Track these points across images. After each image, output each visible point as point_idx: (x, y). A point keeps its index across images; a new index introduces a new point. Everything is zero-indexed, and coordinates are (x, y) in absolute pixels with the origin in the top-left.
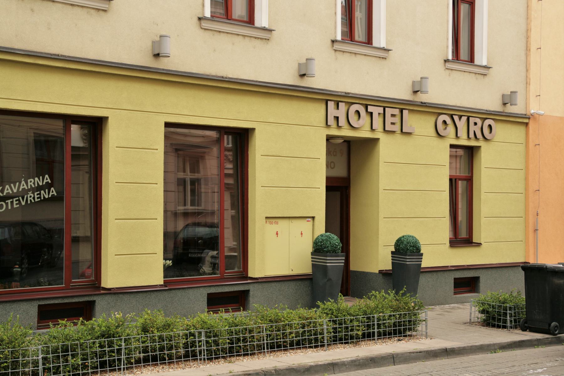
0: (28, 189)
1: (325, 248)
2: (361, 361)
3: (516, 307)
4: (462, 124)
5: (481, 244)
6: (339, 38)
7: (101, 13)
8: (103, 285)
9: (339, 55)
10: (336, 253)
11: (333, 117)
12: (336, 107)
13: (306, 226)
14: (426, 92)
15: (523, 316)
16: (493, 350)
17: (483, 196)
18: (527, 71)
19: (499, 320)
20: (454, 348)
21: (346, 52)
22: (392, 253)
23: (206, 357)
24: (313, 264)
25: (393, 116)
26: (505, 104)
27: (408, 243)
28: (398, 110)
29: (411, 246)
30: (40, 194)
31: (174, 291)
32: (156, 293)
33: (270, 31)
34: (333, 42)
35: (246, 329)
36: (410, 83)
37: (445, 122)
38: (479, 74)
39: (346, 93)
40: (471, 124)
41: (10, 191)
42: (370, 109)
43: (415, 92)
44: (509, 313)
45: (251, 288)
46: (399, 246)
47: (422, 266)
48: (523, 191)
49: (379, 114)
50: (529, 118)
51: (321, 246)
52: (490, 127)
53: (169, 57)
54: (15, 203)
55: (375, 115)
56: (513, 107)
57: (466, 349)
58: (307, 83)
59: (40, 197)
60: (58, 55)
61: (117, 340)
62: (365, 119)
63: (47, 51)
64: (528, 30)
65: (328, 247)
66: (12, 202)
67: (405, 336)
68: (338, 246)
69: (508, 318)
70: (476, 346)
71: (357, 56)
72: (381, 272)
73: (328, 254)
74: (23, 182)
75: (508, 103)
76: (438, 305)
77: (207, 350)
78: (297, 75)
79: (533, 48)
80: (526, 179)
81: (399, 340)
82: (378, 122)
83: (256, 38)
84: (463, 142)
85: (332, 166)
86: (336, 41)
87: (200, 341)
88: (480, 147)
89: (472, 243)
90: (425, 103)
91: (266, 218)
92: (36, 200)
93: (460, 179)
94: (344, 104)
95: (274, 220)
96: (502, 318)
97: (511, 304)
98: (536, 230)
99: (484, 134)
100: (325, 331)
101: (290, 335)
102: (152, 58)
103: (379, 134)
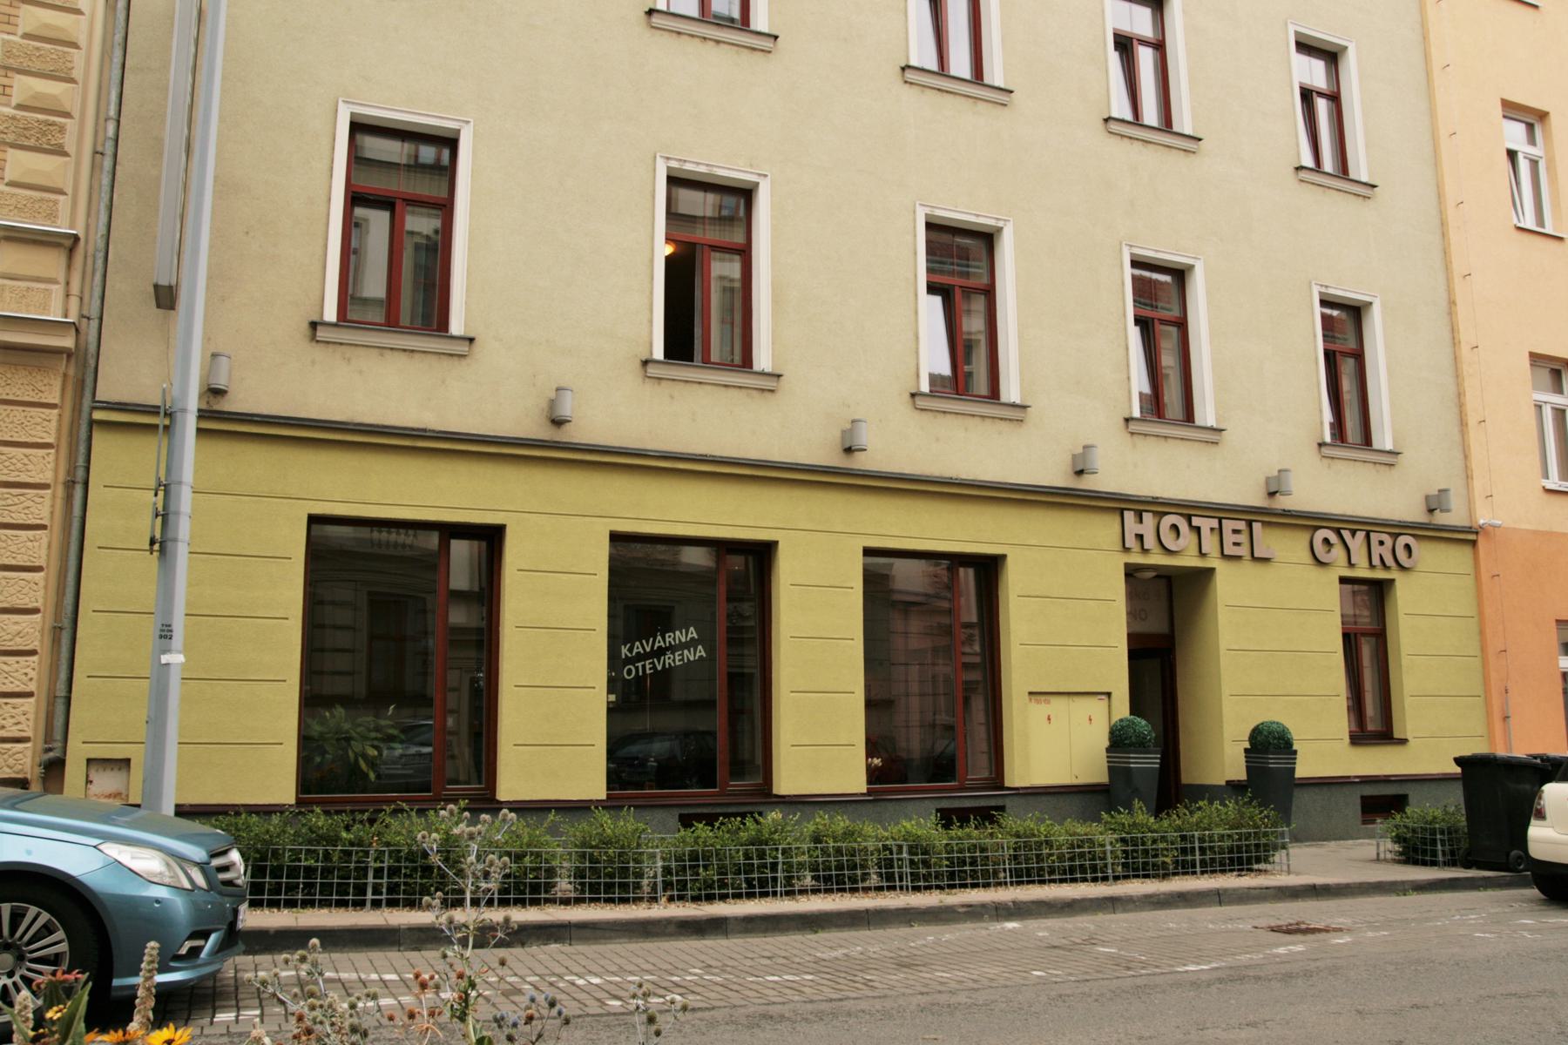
0: (666, 647)
1: (1126, 739)
2: (1162, 896)
3: (1451, 831)
4: (1357, 543)
6: (1137, 413)
7: (767, 394)
8: (775, 791)
9: (1139, 440)
10: (1144, 747)
11: (1134, 536)
12: (1138, 519)
13: (1097, 707)
15: (1464, 845)
16: (1400, 891)
17: (1405, 661)
18: (1466, 457)
19: (1424, 852)
20: (1328, 885)
21: (1149, 435)
22: (1246, 750)
23: (910, 884)
24: (1109, 767)
25: (1236, 532)
26: (1431, 511)
27: (1270, 733)
28: (1244, 522)
29: (1275, 738)
30: (682, 654)
31: (882, 804)
32: (854, 806)
33: (1024, 407)
34: (1127, 420)
35: (975, 846)
36: (1262, 481)
37: (1326, 541)
38: (1380, 463)
39: (1153, 498)
40: (1374, 543)
41: (641, 650)
42: (1196, 521)
43: (1272, 494)
44: (1441, 840)
45: (1008, 803)
46: (1256, 738)
48: (1478, 653)
49: (1212, 529)
50: (1477, 533)
51: (1120, 736)
52: (1408, 547)
53: (865, 450)
54: (648, 667)
55: (1205, 532)
57: (1351, 888)
58: (1088, 483)
59: (682, 660)
60: (706, 456)
61: (771, 849)
62: (1187, 539)
63: (690, 451)
64: (1460, 395)
65: (1131, 737)
66: (644, 666)
67: (1251, 870)
68: (1147, 735)
69: (1439, 847)
70: (1369, 884)
71: (1169, 440)
72: (1228, 783)
73: (1132, 748)
74: (659, 638)
76: (1335, 839)
77: (912, 874)
78: (1070, 471)
79: (1472, 421)
80: (1482, 633)
81: (1239, 875)
82: (1210, 543)
83: (1001, 419)
84: (1363, 572)
85: (1143, 617)
86: (1132, 419)
87: (901, 859)
88: (1392, 581)
89: (1392, 738)
90: (1289, 511)
91: (1030, 693)
92: (678, 663)
93: (1363, 634)
94: (1151, 514)
95: (1043, 698)
96: (1429, 848)
97: (1444, 825)
98: (1506, 718)
99: (1399, 559)
100: (1109, 855)
101: (1048, 858)
102: (842, 455)
103: (1214, 562)
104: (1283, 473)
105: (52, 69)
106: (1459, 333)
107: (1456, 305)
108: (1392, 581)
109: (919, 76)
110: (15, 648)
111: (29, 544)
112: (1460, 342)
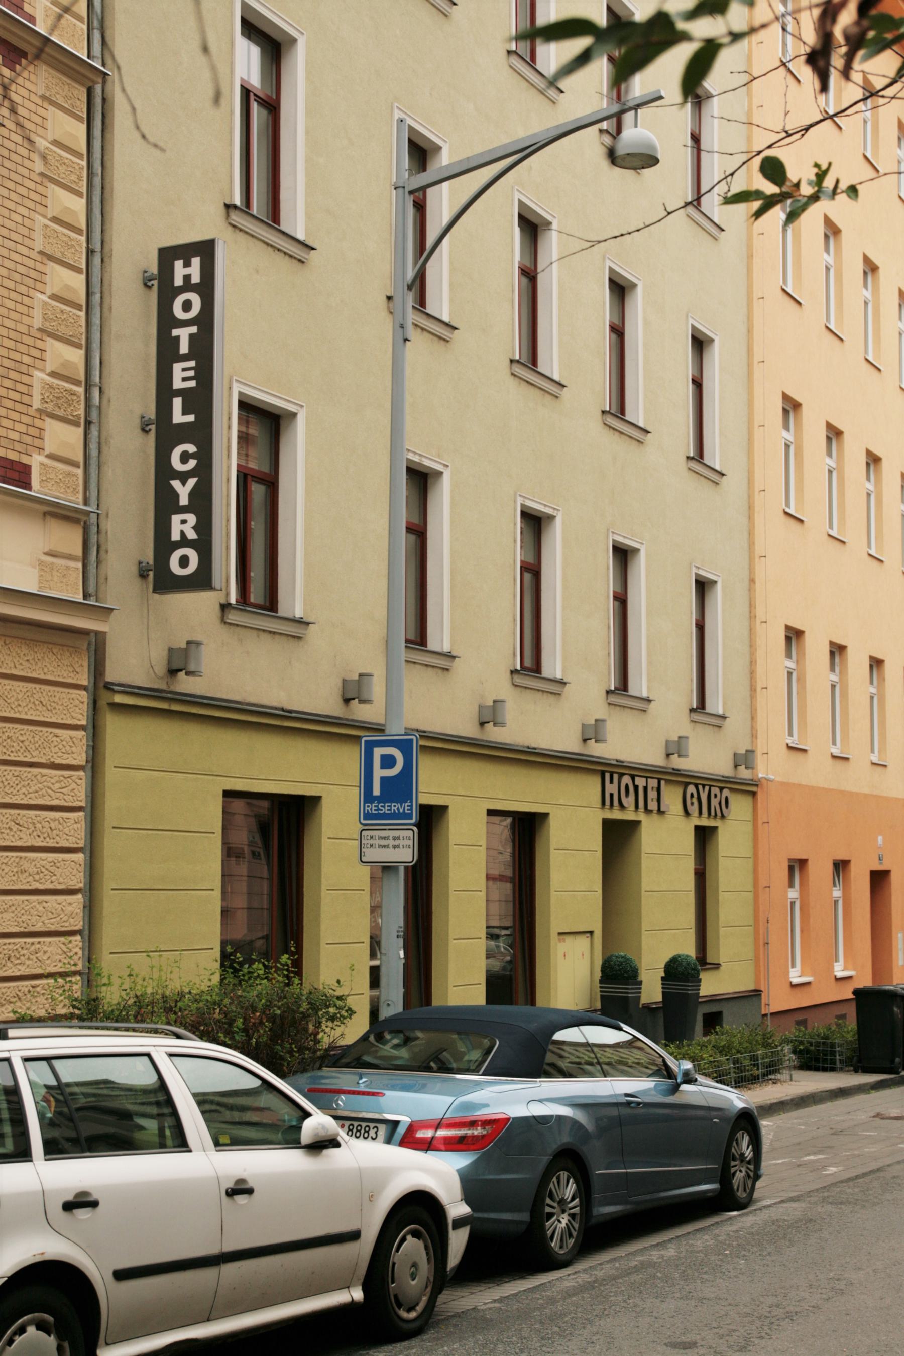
5: (719, 964)
14: (503, 724)
17: (723, 897)
19: (825, 1061)
26: (347, 701)
38: (709, 724)
47: (701, 995)
48: (751, 889)
56: (682, 759)
75: (488, 722)
88: (716, 828)
104: (193, 646)
105: (71, 334)
106: (755, 608)
107: (755, 583)
108: (716, 828)
109: (267, 232)
110: (69, 929)
111: (75, 826)
112: (755, 617)
